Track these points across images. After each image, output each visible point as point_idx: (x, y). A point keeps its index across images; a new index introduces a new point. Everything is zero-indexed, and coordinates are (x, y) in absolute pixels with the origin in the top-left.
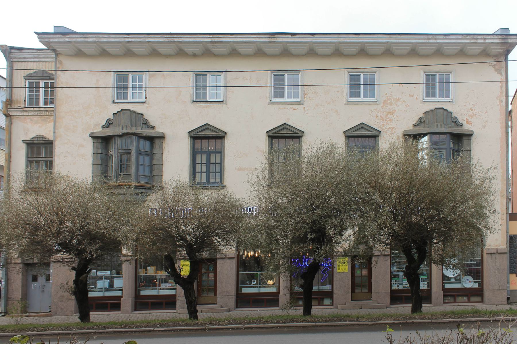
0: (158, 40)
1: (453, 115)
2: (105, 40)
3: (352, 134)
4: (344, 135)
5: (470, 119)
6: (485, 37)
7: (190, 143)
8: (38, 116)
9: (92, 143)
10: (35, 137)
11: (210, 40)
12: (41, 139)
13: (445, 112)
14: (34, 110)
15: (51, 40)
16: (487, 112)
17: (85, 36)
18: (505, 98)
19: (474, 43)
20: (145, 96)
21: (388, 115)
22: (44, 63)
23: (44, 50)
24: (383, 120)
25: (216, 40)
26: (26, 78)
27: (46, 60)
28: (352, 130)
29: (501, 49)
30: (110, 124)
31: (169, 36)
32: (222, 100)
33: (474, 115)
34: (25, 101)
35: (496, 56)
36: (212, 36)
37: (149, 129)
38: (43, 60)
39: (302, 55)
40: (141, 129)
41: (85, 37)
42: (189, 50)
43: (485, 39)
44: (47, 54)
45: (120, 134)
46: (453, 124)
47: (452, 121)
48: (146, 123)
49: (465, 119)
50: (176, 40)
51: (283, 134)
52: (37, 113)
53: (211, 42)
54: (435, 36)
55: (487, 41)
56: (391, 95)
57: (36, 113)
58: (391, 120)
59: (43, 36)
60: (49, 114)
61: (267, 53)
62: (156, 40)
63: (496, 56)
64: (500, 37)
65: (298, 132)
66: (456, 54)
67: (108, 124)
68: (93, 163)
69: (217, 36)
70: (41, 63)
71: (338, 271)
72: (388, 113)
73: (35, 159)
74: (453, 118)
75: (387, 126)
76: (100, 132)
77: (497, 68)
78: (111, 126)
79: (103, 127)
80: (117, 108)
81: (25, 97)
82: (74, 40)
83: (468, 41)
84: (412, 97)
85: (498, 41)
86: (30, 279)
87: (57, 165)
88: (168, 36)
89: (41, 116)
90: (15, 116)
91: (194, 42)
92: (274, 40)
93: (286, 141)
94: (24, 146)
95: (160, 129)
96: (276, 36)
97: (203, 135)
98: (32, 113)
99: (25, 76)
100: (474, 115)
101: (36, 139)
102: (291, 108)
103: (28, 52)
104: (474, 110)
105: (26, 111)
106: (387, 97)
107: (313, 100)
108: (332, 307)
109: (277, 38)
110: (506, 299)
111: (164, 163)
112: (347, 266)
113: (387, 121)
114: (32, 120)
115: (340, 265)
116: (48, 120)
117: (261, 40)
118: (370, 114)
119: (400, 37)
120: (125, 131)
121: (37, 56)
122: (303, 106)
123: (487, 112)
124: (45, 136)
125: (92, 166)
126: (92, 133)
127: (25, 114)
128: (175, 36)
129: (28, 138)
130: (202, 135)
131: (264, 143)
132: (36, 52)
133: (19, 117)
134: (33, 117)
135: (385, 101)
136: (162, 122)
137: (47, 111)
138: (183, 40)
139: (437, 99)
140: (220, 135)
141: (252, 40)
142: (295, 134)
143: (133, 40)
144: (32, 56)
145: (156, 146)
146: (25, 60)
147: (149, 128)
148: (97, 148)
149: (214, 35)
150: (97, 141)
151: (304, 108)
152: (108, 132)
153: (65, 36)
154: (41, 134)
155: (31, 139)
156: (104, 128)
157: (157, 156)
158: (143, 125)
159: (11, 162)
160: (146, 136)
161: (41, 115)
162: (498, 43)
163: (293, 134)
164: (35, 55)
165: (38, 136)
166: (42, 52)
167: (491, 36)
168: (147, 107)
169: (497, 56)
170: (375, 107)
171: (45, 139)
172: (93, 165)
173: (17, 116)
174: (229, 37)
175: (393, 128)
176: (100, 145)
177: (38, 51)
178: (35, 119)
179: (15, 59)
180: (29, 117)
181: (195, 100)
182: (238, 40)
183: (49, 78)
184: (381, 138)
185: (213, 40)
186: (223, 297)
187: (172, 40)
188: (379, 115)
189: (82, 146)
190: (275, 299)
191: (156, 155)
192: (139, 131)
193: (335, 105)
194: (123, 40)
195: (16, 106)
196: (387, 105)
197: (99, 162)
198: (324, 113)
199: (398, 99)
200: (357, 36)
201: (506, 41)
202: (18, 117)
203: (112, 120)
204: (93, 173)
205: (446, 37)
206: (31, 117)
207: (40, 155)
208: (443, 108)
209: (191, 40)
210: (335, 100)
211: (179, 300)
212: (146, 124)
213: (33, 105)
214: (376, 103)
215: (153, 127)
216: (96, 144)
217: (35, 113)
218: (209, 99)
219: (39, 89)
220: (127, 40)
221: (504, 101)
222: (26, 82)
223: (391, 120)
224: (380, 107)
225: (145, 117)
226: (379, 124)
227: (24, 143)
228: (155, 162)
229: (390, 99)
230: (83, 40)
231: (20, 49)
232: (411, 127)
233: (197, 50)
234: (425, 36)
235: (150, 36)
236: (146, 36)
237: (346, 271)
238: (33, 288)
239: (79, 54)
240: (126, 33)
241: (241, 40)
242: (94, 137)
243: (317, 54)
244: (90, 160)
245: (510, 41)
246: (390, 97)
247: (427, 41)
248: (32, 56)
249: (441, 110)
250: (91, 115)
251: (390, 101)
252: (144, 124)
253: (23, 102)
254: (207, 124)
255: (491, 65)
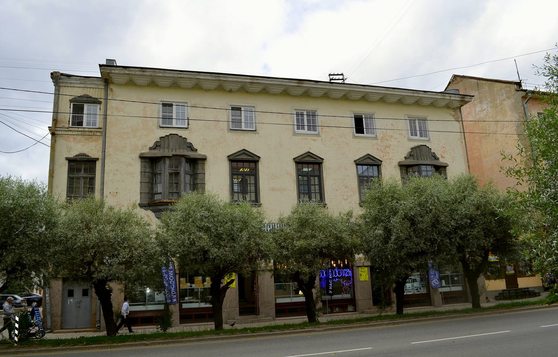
0: (207, 78)
1: (432, 151)
2: (161, 75)
3: (361, 163)
4: (354, 163)
5: (443, 154)
6: (451, 95)
7: (229, 165)
8: (81, 136)
9: (140, 163)
10: (79, 155)
11: (250, 81)
12: (84, 157)
13: (427, 149)
14: (79, 130)
15: (112, 72)
16: (453, 150)
17: (144, 70)
18: (464, 140)
19: (443, 99)
20: (188, 123)
21: (386, 148)
22: (89, 89)
23: (91, 78)
24: (383, 152)
25: (255, 81)
26: (71, 101)
27: (91, 86)
28: (361, 160)
29: (460, 104)
30: (157, 146)
31: (217, 75)
32: (255, 130)
33: (445, 151)
34: (69, 121)
35: (454, 109)
36: (252, 78)
37: (193, 152)
38: (88, 86)
39: (299, 96)
40: (187, 152)
41: (143, 71)
42: (228, 87)
43: (450, 97)
44: (93, 81)
45: (171, 155)
46: (433, 158)
47: (432, 156)
48: (191, 147)
49: (440, 154)
50: (222, 79)
51: (307, 161)
52: (81, 132)
53: (250, 82)
54: (418, 92)
55: (452, 98)
56: (386, 133)
57: (80, 133)
58: (388, 153)
59: (106, 68)
60: (92, 134)
61: (159, 85)
62: (205, 78)
63: (454, 109)
64: (460, 96)
65: (320, 160)
66: (259, 92)
67: (157, 146)
68: (140, 181)
69: (257, 78)
70: (86, 88)
71: (361, 280)
72: (386, 147)
73: (76, 175)
74: (432, 153)
75: (386, 158)
76: (149, 153)
77: (456, 117)
78: (158, 148)
79: (150, 148)
80: (164, 133)
81: (70, 118)
82: (133, 73)
83: (440, 97)
84: (401, 135)
85: (459, 99)
86: (66, 294)
87: (106, 182)
88: (215, 75)
89: (84, 136)
90: (59, 135)
91: (236, 82)
92: (300, 85)
93: (308, 166)
94: (66, 162)
95: (201, 151)
96: (303, 82)
97: (241, 159)
98: (76, 133)
99: (70, 99)
100: (445, 151)
101: (80, 157)
102: (311, 139)
103: (76, 79)
104: (445, 147)
105: (71, 131)
106: (384, 134)
107: (328, 133)
108: (355, 313)
109: (304, 83)
110: (485, 298)
111: (206, 182)
112: (368, 275)
113: (386, 153)
114: (75, 139)
115: (362, 274)
116: (91, 140)
117: (291, 84)
118: (373, 147)
119: (394, 90)
120: (174, 153)
121: (83, 82)
122: (321, 138)
123: (453, 150)
124: (87, 154)
125: (139, 183)
126: (142, 154)
127: (69, 133)
128: (222, 76)
129: (72, 155)
130: (240, 159)
131: (292, 168)
132: (83, 79)
133: (63, 135)
134: (76, 136)
135: (382, 137)
136: (203, 146)
137: (91, 131)
138: (228, 79)
139: (418, 137)
140: (256, 159)
141: (284, 83)
142: (317, 161)
143: (185, 76)
144: (79, 82)
145: (199, 167)
146: (74, 85)
147: (192, 150)
148: (145, 167)
149: (200, 73)
150: (144, 161)
151: (322, 139)
152: (157, 153)
153: (126, 69)
154: (84, 152)
155: (74, 157)
156: (151, 149)
157: (200, 176)
158: (188, 148)
159: (54, 178)
160: (192, 158)
161: (84, 135)
162: (458, 100)
163: (316, 161)
164: (82, 82)
165: (81, 154)
166: (89, 79)
167: (454, 95)
168: (190, 132)
169: (454, 109)
170: (375, 142)
171: (88, 156)
172: (141, 183)
173: (61, 135)
174: (266, 80)
175: (390, 159)
176: (147, 165)
177: (86, 79)
178: (78, 138)
179: (62, 84)
180: (72, 136)
181: (231, 128)
182: (273, 83)
183: (93, 102)
184: (382, 167)
185: (253, 81)
186: (264, 307)
187: (219, 79)
188: (379, 148)
189: (130, 165)
190: (337, 309)
191: (199, 175)
192: (186, 153)
193: (346, 139)
194: (176, 76)
195: (61, 126)
196: (384, 141)
197: (147, 180)
198: (338, 144)
199: (392, 136)
200: (363, 87)
201: (464, 100)
202: (62, 136)
203: (159, 142)
204: (141, 190)
205: (425, 93)
206: (74, 136)
207: (81, 172)
208: (426, 145)
209: (235, 80)
210: (346, 135)
211: (224, 311)
212: (190, 147)
213: (91, 126)
214: (376, 138)
215: (196, 150)
216: (143, 164)
217: (79, 132)
218: (243, 128)
219: (163, 116)
220: (180, 76)
221: (464, 142)
222: (70, 105)
223: (388, 153)
224: (379, 141)
225: (188, 141)
226: (380, 155)
227: (67, 160)
228: (199, 181)
229: (386, 136)
230: (142, 73)
231: (69, 76)
232: (403, 159)
233: (235, 87)
234: (411, 91)
235: (200, 74)
236: (197, 74)
237: (367, 280)
238: (69, 303)
239: (131, 83)
240: (140, 67)
241: (276, 83)
242: (143, 158)
243: (136, 84)
244: (137, 178)
245: (466, 100)
246: (385, 134)
247: (412, 95)
248: (79, 82)
249: (425, 147)
250: (139, 137)
251: (386, 137)
252: (188, 147)
253: (68, 122)
254: (244, 149)
255: (451, 115)
